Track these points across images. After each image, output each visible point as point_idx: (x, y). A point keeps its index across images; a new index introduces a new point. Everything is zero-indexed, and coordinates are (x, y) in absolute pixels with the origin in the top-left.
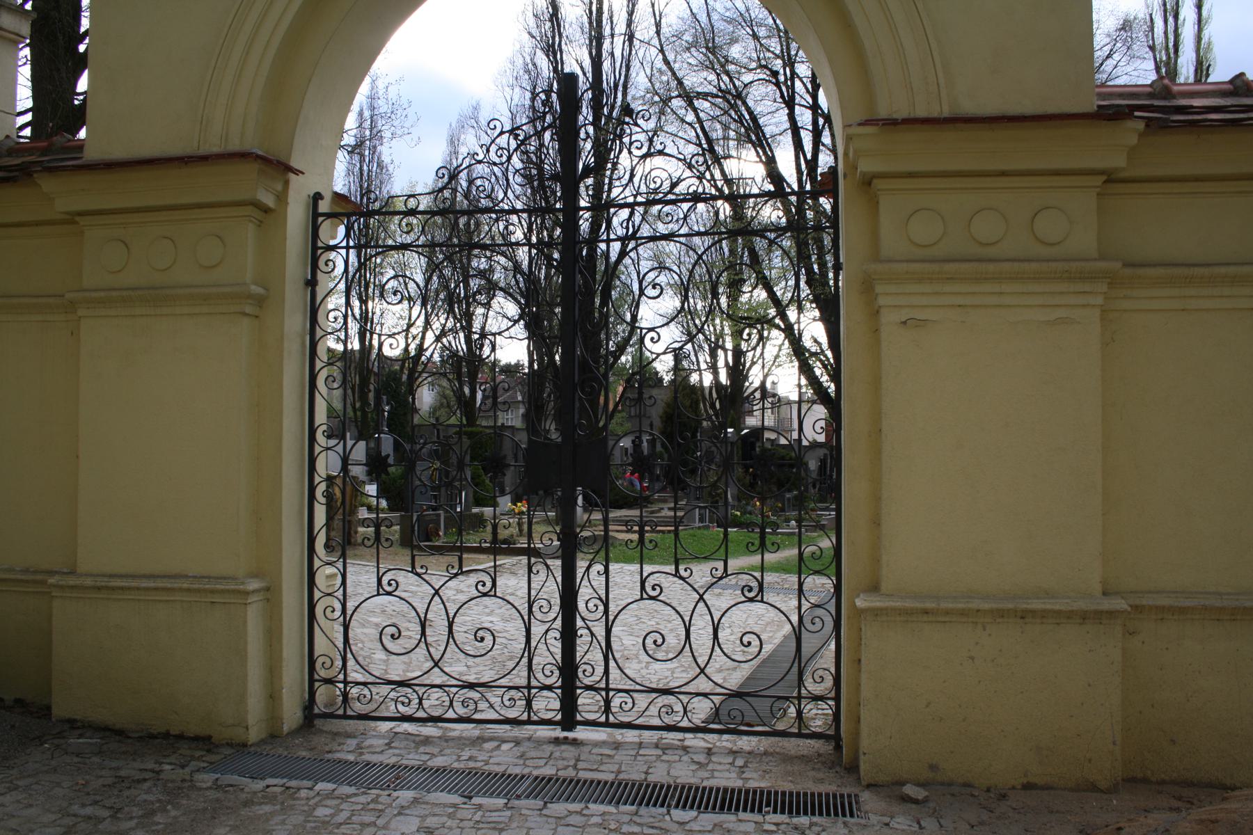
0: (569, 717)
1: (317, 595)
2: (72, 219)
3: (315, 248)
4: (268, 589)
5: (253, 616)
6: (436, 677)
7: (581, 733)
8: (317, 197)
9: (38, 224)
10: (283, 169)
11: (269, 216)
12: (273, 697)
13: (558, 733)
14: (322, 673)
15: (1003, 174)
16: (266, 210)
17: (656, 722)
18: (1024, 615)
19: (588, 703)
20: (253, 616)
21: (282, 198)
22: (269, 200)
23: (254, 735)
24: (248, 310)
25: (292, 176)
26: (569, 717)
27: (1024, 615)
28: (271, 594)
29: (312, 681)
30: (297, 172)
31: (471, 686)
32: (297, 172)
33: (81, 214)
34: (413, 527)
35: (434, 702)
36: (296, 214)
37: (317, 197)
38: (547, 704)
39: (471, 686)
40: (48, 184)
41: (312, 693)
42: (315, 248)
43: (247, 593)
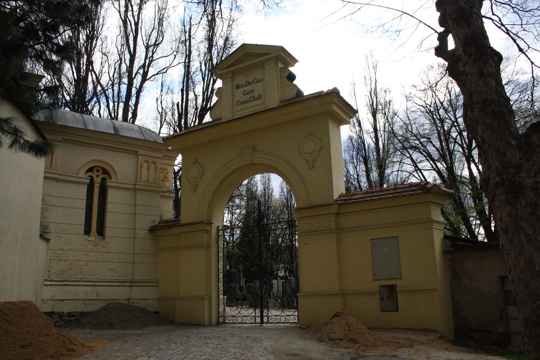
0: (262, 322)
1: (220, 300)
2: (178, 234)
3: (218, 236)
4: (210, 298)
5: (206, 303)
6: (239, 315)
7: (264, 325)
8: (218, 227)
9: (384, 208)
10: (210, 223)
11: (209, 232)
12: (210, 318)
13: (260, 324)
14: (220, 315)
15: (319, 215)
16: (208, 231)
17: (275, 322)
18: (324, 295)
19: (265, 320)
20: (206, 303)
21: (211, 228)
22: (209, 229)
23: (206, 324)
24: (206, 248)
25: (213, 224)
26: (262, 322)
27: (324, 295)
28: (210, 299)
29: (219, 316)
30: (213, 224)
31: (245, 316)
32: (213, 224)
33: (180, 233)
34: (285, 303)
35: (239, 320)
36: (214, 231)
37: (218, 227)
38: (258, 320)
39: (245, 316)
40: (175, 229)
41: (219, 319)
42: (218, 236)
43: (205, 298)
